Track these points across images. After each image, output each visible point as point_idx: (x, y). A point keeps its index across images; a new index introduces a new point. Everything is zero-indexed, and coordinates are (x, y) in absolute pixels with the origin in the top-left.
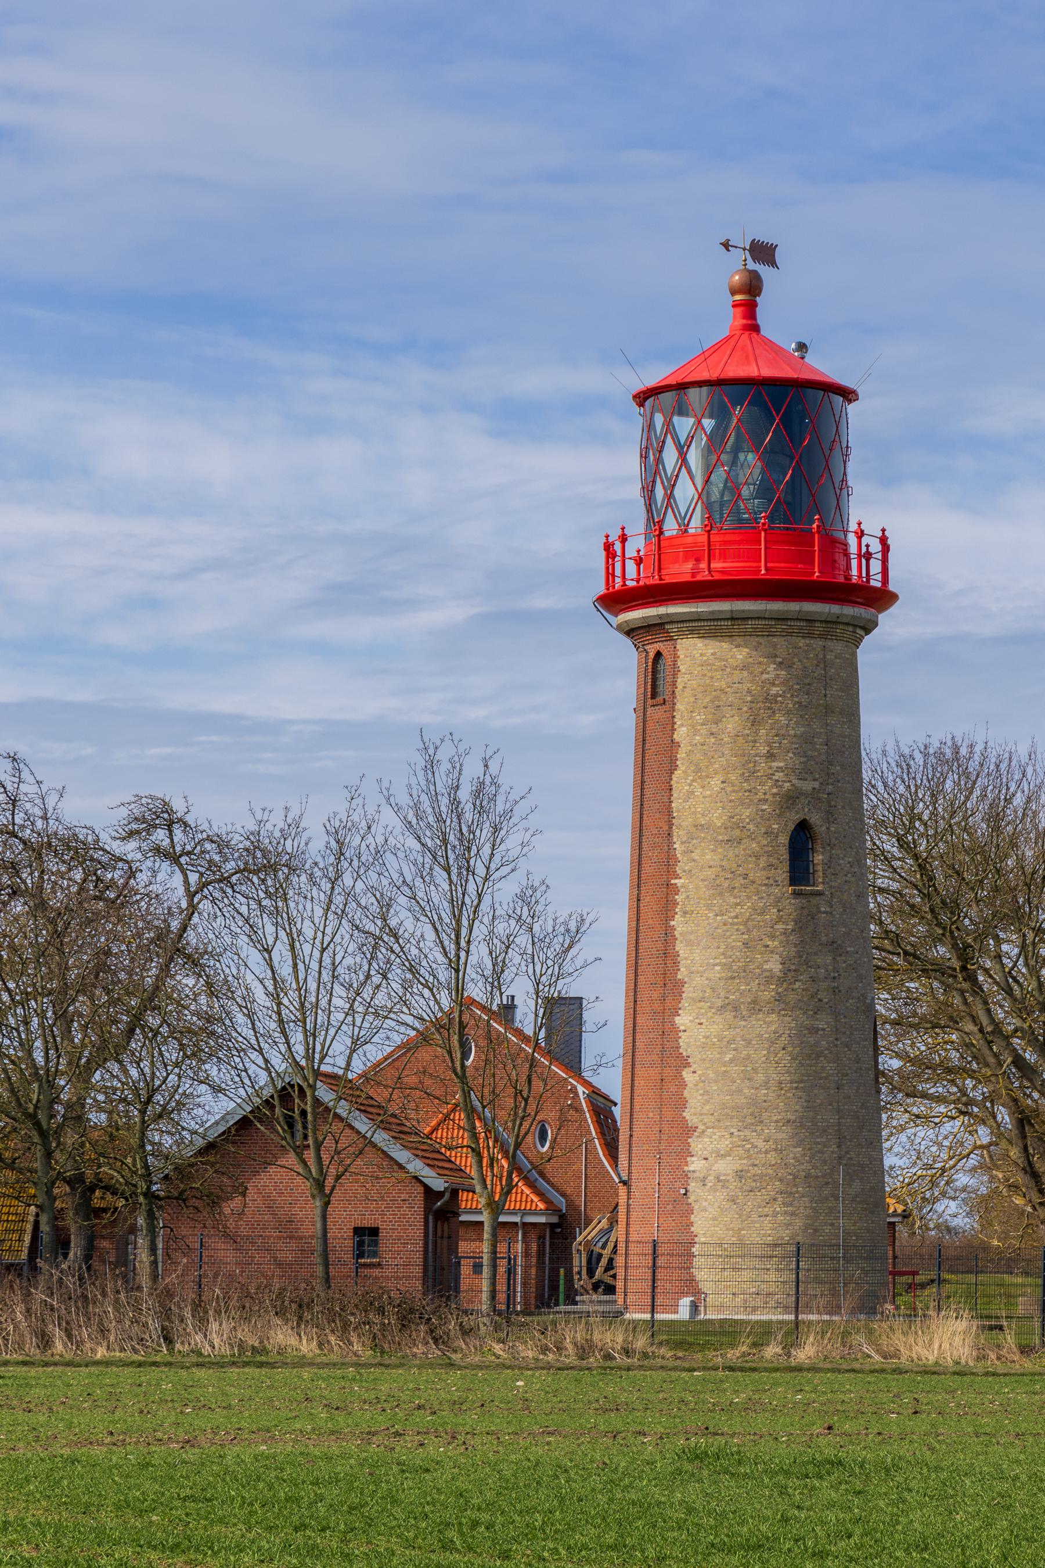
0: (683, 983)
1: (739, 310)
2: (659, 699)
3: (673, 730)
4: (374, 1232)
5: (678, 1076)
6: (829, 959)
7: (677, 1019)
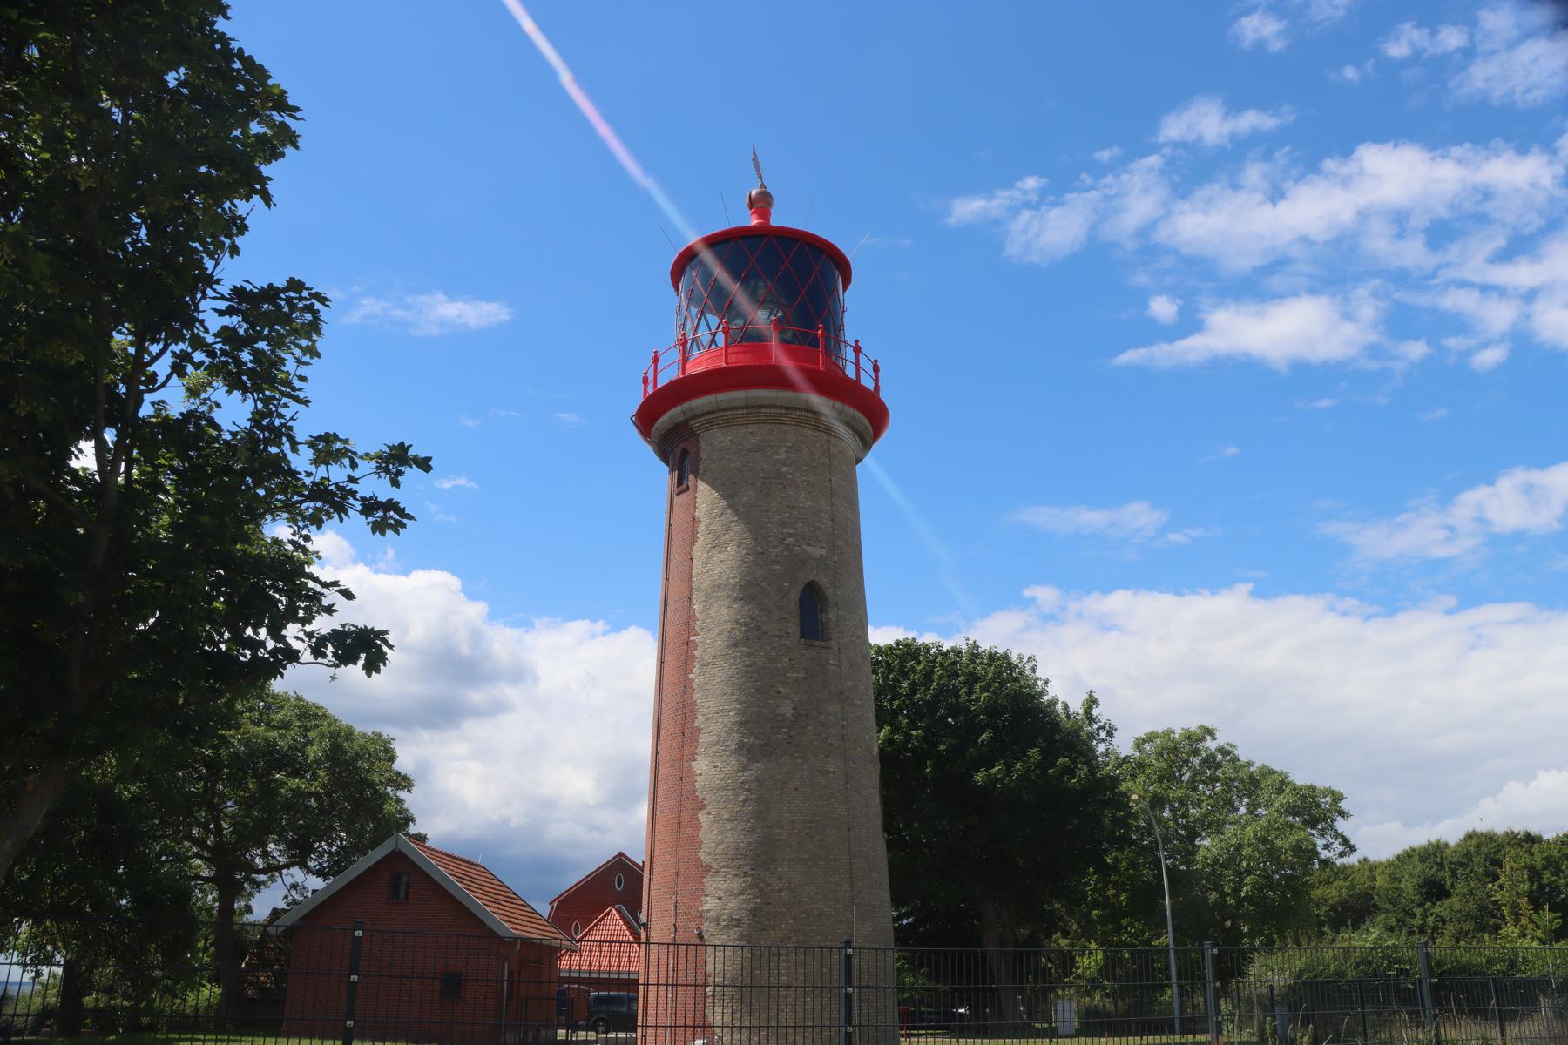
0: (699, 730)
5: (694, 818)
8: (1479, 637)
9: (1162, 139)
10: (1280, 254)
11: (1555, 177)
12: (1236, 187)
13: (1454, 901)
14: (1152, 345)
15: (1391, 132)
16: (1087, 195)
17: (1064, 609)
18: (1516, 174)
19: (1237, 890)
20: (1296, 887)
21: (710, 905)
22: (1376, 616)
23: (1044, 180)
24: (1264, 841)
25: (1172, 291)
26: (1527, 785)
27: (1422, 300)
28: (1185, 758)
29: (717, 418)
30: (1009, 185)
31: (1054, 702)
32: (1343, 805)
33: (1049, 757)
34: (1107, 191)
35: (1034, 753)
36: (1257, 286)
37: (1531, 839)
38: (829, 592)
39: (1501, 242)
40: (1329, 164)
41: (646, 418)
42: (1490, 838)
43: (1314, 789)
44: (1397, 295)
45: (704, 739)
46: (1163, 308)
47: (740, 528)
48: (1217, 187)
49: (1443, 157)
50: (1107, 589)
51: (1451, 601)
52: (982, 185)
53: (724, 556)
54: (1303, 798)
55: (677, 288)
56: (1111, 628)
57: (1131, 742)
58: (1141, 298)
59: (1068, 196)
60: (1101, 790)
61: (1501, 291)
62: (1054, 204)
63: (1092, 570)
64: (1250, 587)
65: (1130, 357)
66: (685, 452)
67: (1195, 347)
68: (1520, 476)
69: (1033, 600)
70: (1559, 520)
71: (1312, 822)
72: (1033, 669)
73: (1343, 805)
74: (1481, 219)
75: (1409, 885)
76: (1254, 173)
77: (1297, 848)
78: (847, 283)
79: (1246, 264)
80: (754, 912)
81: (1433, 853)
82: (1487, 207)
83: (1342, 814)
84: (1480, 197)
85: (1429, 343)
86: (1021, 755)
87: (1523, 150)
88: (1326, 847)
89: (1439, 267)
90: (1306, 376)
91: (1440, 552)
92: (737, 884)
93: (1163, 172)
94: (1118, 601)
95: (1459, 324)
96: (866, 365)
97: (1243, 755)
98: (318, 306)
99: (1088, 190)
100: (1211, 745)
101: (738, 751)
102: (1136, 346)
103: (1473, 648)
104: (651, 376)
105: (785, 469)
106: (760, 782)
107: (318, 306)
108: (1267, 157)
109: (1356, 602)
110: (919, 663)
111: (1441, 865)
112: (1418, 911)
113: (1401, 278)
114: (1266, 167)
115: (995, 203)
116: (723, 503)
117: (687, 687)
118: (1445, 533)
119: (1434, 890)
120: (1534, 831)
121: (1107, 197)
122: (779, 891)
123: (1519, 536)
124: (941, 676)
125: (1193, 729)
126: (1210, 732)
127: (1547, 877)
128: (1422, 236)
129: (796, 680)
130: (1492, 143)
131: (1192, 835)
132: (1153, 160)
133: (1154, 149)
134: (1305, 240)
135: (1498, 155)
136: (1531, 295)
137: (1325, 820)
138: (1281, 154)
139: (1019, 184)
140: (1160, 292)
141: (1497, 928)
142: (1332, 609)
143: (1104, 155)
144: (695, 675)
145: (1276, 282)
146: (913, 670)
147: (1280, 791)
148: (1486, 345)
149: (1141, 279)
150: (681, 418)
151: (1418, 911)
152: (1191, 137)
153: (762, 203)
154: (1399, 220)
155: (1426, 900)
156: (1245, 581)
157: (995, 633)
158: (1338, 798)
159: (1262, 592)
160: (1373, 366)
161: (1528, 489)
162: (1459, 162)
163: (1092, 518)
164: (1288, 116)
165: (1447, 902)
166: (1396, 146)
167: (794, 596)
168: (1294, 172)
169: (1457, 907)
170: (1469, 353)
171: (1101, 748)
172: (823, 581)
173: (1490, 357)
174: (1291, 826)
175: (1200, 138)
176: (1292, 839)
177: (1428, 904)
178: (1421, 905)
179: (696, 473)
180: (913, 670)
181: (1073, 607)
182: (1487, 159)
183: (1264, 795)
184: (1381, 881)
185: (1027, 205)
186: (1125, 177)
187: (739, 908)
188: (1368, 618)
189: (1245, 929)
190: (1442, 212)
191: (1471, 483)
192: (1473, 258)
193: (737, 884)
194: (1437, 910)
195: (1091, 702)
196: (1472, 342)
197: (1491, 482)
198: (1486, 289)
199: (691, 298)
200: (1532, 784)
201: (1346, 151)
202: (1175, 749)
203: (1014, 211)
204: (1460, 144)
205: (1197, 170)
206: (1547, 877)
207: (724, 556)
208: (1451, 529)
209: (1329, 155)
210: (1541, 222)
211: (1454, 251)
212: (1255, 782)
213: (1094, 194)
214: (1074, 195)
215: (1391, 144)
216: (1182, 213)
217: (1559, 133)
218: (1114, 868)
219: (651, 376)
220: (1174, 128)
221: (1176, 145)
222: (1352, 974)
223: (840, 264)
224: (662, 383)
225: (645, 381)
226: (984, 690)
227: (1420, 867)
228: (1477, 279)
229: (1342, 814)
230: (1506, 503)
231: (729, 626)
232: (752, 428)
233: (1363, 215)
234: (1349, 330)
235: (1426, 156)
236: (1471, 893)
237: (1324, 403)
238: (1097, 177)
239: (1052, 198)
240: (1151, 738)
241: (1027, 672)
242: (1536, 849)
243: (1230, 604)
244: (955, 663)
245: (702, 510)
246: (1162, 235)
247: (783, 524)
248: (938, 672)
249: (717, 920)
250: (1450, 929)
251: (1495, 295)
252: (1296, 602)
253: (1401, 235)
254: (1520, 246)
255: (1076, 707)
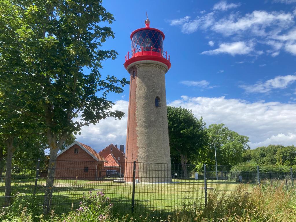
0: (137, 123)
1: (119, 148)
2: (134, 78)
3: (136, 82)
4: (87, 168)
5: (136, 138)
6: (162, 119)
7: (136, 129)
8: (269, 108)
9: (214, 9)
10: (235, 34)
11: (292, 18)
12: (228, 19)
13: (267, 158)
14: (209, 50)
15: (260, 8)
16: (198, 20)
17: (188, 100)
18: (285, 17)
19: (228, 154)
20: (239, 153)
21: (139, 154)
22: (249, 103)
23: (190, 17)
24: (234, 145)
25: (213, 40)
26: (276, 136)
27: (263, 43)
28: (219, 129)
29: (140, 65)
30: (183, 17)
31: (194, 119)
32: (249, 140)
33: (194, 129)
34: (202, 19)
35: (192, 128)
36: (230, 39)
37: (282, 147)
38: (160, 98)
39: (280, 31)
40: (247, 15)
41: (127, 64)
42: (273, 146)
43: (243, 136)
44: (258, 42)
45: (138, 124)
46: (211, 43)
47: (145, 86)
48: (224, 19)
49: (270, 14)
50: (197, 97)
51: (264, 101)
52: (178, 18)
53: (142, 91)
54: (241, 138)
55: (132, 39)
56: (198, 104)
57: (209, 126)
58: (208, 41)
59: (194, 20)
60: (204, 135)
61: (279, 41)
62: (192, 22)
63: (194, 93)
64: (224, 97)
65: (204, 53)
66: (134, 71)
67: (217, 51)
68: (279, 78)
69: (183, 98)
70: (286, 86)
71: (243, 143)
72: (191, 112)
73: (249, 140)
74: (277, 26)
75: (258, 155)
76: (231, 17)
77: (240, 147)
78: (164, 39)
79: (228, 35)
80: (147, 156)
81: (263, 149)
82: (278, 24)
83: (248, 141)
84: (277, 22)
85: (263, 51)
86: (189, 128)
87: (286, 13)
88: (245, 147)
89: (267, 36)
90: (238, 57)
91: (262, 92)
92: (144, 151)
93: (213, 16)
94: (199, 99)
95: (270, 47)
96: (168, 56)
97: (229, 129)
98: (116, 55)
99: (198, 19)
100: (223, 127)
101: (144, 126)
102: (205, 51)
103: (267, 110)
104: (127, 56)
105: (153, 75)
106: (148, 132)
107: (116, 55)
108: (234, 13)
109: (245, 100)
110: (171, 110)
111: (264, 151)
112: (259, 159)
113: (259, 38)
114: (234, 15)
115: (180, 21)
116: (141, 81)
117: (135, 115)
118: (264, 88)
119: (263, 155)
120: (283, 146)
121: (202, 21)
122: (152, 152)
123: (278, 89)
124: (175, 113)
125: (220, 124)
126: (223, 125)
127: (285, 154)
128: (264, 30)
129: (155, 114)
130: (280, 11)
131: (220, 144)
132: (212, 13)
133: (212, 11)
134: (241, 30)
135: (281, 14)
136: (285, 42)
137: (245, 142)
138: (237, 13)
139: (185, 18)
140: (211, 40)
141: (275, 163)
142: (240, 102)
143: (202, 12)
144: (136, 113)
145: (234, 38)
146: (170, 111)
147: (237, 137)
148: (275, 52)
149: (208, 37)
150: (133, 65)
151: (259, 159)
152: (220, 9)
153: (148, 23)
154: (260, 26)
155: (261, 157)
156: (224, 96)
157: (184, 106)
158: (248, 138)
159: (227, 98)
160: (252, 55)
161: (281, 80)
162: (273, 15)
163: (195, 83)
164: (240, 5)
165: (265, 158)
166: (261, 11)
167: (154, 99)
168: (240, 16)
169: (267, 159)
170: (271, 53)
171: (203, 127)
172: (159, 96)
173: (276, 54)
174: (239, 143)
175: (221, 9)
176: (239, 145)
177: (261, 158)
178: (260, 158)
179: (136, 75)
180: (170, 111)
181: (190, 100)
182: (279, 14)
183: (234, 137)
184: (252, 153)
185: (186, 22)
186: (206, 17)
187: (145, 155)
188: (247, 104)
189: (230, 161)
190: (269, 25)
191: (269, 79)
192: (274, 35)
193: (144, 151)
194: (263, 159)
195: (202, 118)
196: (272, 51)
197: (273, 78)
198: (276, 41)
199: (135, 41)
200: (277, 136)
201: (251, 12)
202: (217, 128)
203: (184, 23)
204: (274, 11)
205: (221, 16)
206: (285, 154)
207: (142, 91)
208: (265, 87)
209: (247, 13)
210: (288, 27)
211: (270, 33)
212: (232, 135)
213: (199, 20)
214: (196, 20)
215: (260, 11)
216: (217, 24)
217: (294, 9)
218: (205, 149)
219: (127, 56)
220: (216, 7)
221: (216, 10)
222: (251, 170)
223: (163, 36)
224: (129, 59)
225: (126, 57)
226: (182, 115)
227: (260, 151)
228: (274, 38)
229: (248, 141)
230: (276, 83)
231: (143, 104)
232: (147, 67)
233: (253, 25)
234: (248, 48)
235: (267, 13)
236: (270, 156)
237: (241, 62)
238: (200, 17)
239: (191, 21)
240: (212, 125)
241: (190, 113)
242: (283, 149)
243: (220, 100)
244: (177, 111)
245: (137, 82)
246: (213, 28)
247: (153, 86)
248: (174, 112)
249: (140, 157)
250: (265, 163)
251: (278, 42)
252: (233, 100)
253: (260, 29)
254: (284, 32)
255: (199, 119)
